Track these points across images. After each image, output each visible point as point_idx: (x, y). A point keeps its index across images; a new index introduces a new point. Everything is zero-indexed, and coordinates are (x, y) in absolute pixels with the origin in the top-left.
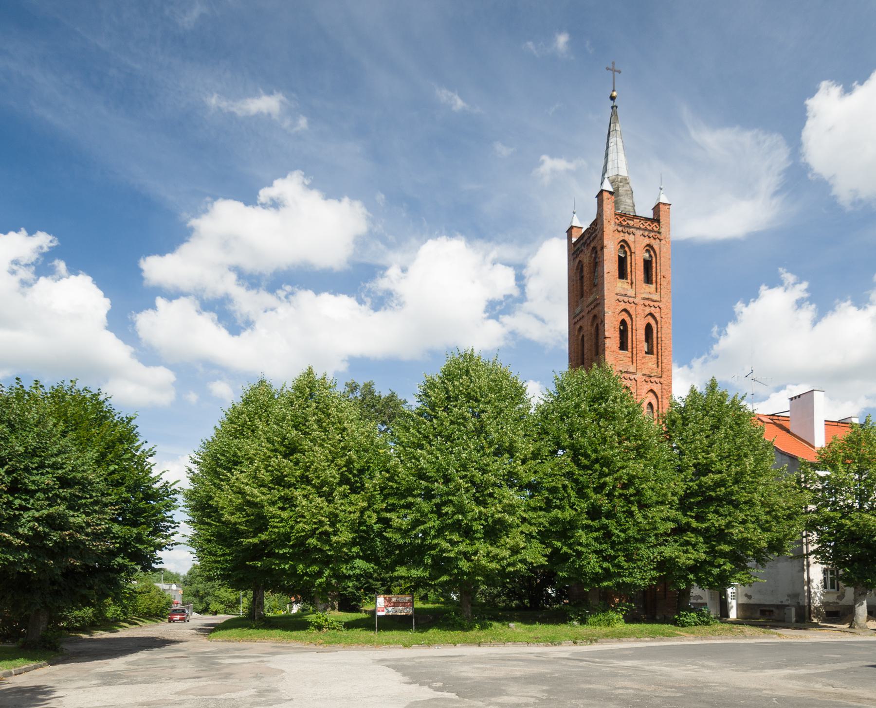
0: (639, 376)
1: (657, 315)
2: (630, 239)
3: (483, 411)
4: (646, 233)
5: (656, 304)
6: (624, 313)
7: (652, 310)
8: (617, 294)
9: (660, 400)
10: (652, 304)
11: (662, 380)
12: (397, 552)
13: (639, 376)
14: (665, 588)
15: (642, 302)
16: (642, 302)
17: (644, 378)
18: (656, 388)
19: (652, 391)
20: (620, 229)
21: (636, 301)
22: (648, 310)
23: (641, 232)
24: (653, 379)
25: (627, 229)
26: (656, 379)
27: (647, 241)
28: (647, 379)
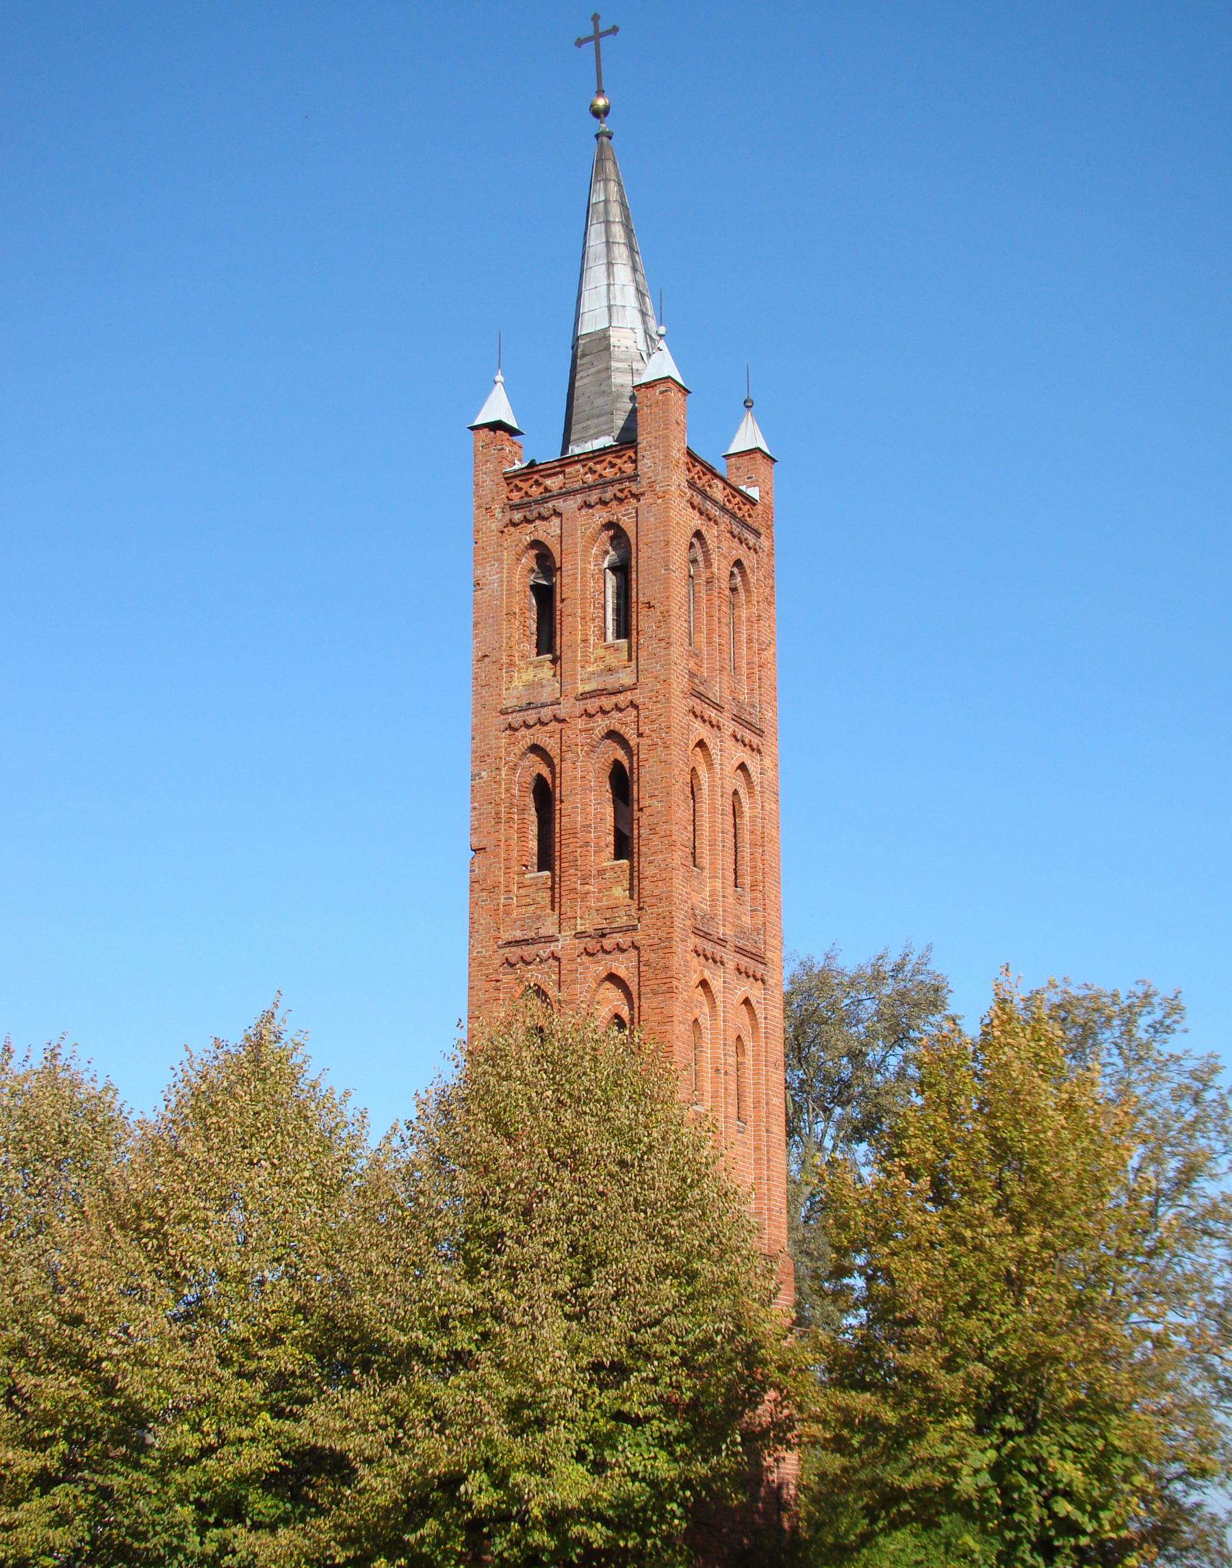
0: (565, 944)
1: (629, 733)
2: (548, 531)
3: (361, 1270)
4: (594, 497)
5: (622, 699)
6: (608, 985)
7: (614, 721)
8: (504, 712)
9: (636, 1001)
10: (608, 703)
11: (638, 937)
12: (1096, 1345)
13: (565, 944)
14: (885, 1057)
15: (580, 707)
16: (580, 707)
17: (580, 945)
18: (623, 966)
19: (612, 978)
20: (517, 516)
21: (562, 711)
22: (601, 724)
23: (579, 499)
24: (608, 943)
25: (536, 510)
26: (619, 938)
27: (600, 516)
28: (592, 945)
